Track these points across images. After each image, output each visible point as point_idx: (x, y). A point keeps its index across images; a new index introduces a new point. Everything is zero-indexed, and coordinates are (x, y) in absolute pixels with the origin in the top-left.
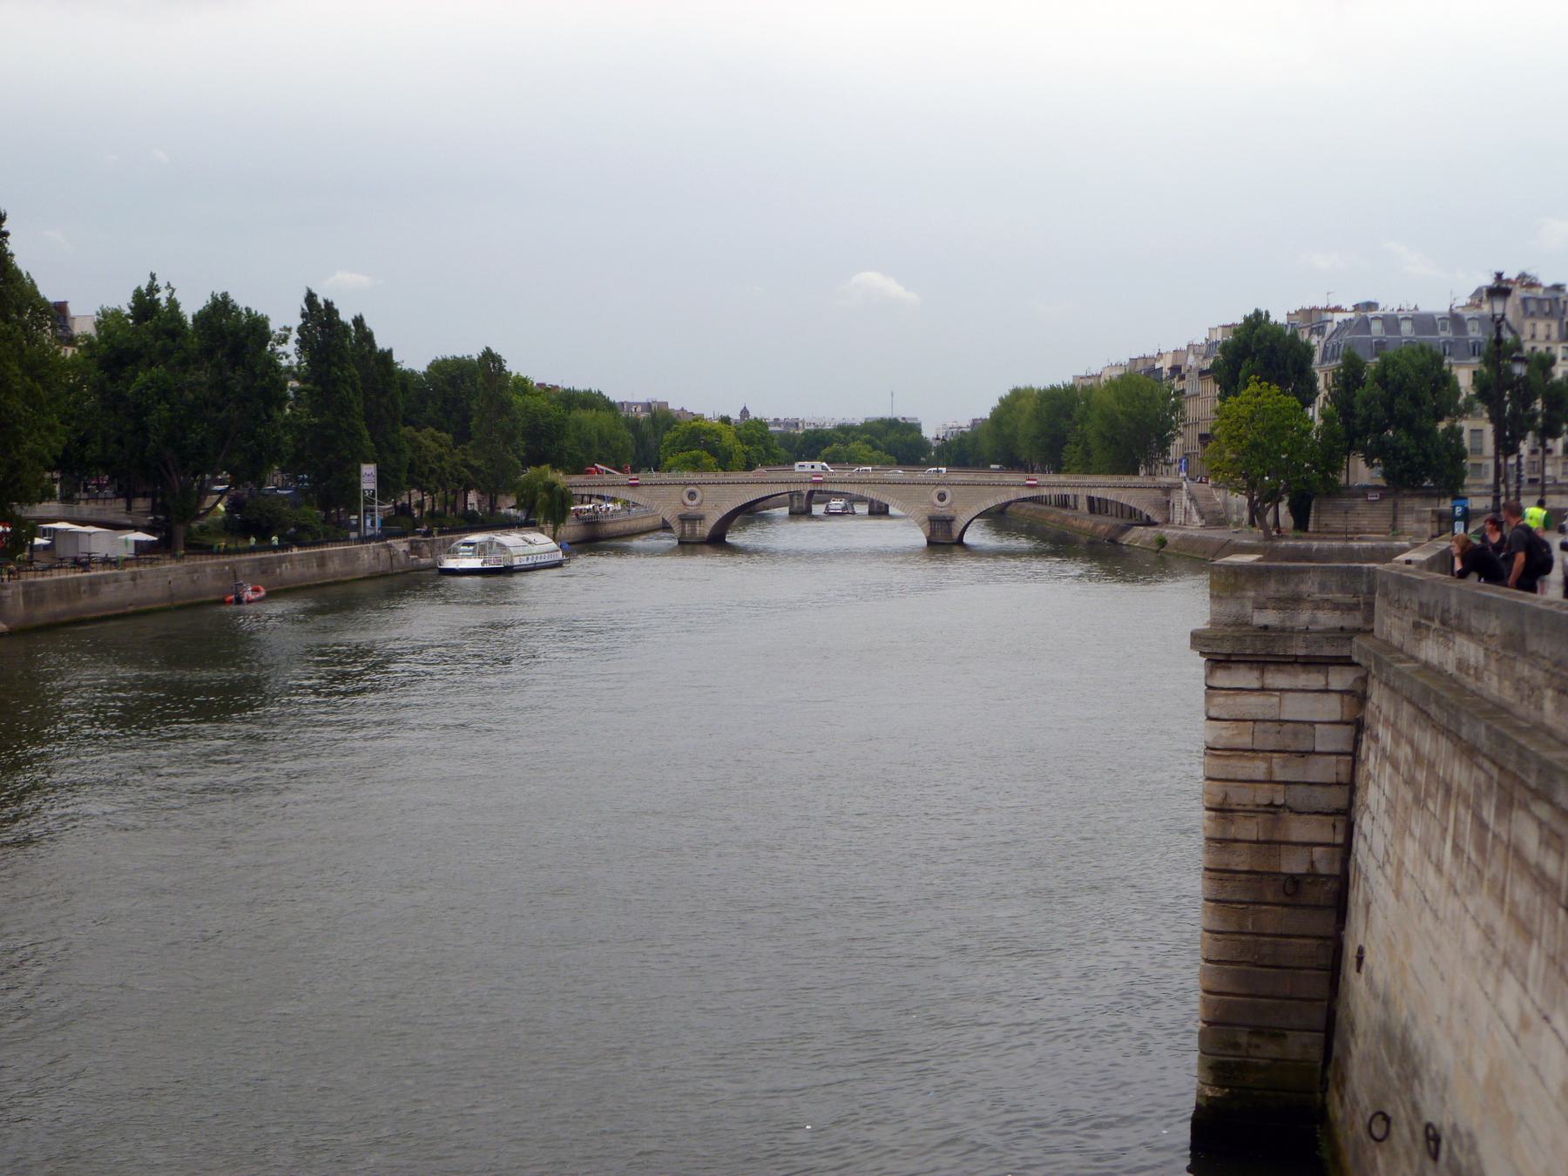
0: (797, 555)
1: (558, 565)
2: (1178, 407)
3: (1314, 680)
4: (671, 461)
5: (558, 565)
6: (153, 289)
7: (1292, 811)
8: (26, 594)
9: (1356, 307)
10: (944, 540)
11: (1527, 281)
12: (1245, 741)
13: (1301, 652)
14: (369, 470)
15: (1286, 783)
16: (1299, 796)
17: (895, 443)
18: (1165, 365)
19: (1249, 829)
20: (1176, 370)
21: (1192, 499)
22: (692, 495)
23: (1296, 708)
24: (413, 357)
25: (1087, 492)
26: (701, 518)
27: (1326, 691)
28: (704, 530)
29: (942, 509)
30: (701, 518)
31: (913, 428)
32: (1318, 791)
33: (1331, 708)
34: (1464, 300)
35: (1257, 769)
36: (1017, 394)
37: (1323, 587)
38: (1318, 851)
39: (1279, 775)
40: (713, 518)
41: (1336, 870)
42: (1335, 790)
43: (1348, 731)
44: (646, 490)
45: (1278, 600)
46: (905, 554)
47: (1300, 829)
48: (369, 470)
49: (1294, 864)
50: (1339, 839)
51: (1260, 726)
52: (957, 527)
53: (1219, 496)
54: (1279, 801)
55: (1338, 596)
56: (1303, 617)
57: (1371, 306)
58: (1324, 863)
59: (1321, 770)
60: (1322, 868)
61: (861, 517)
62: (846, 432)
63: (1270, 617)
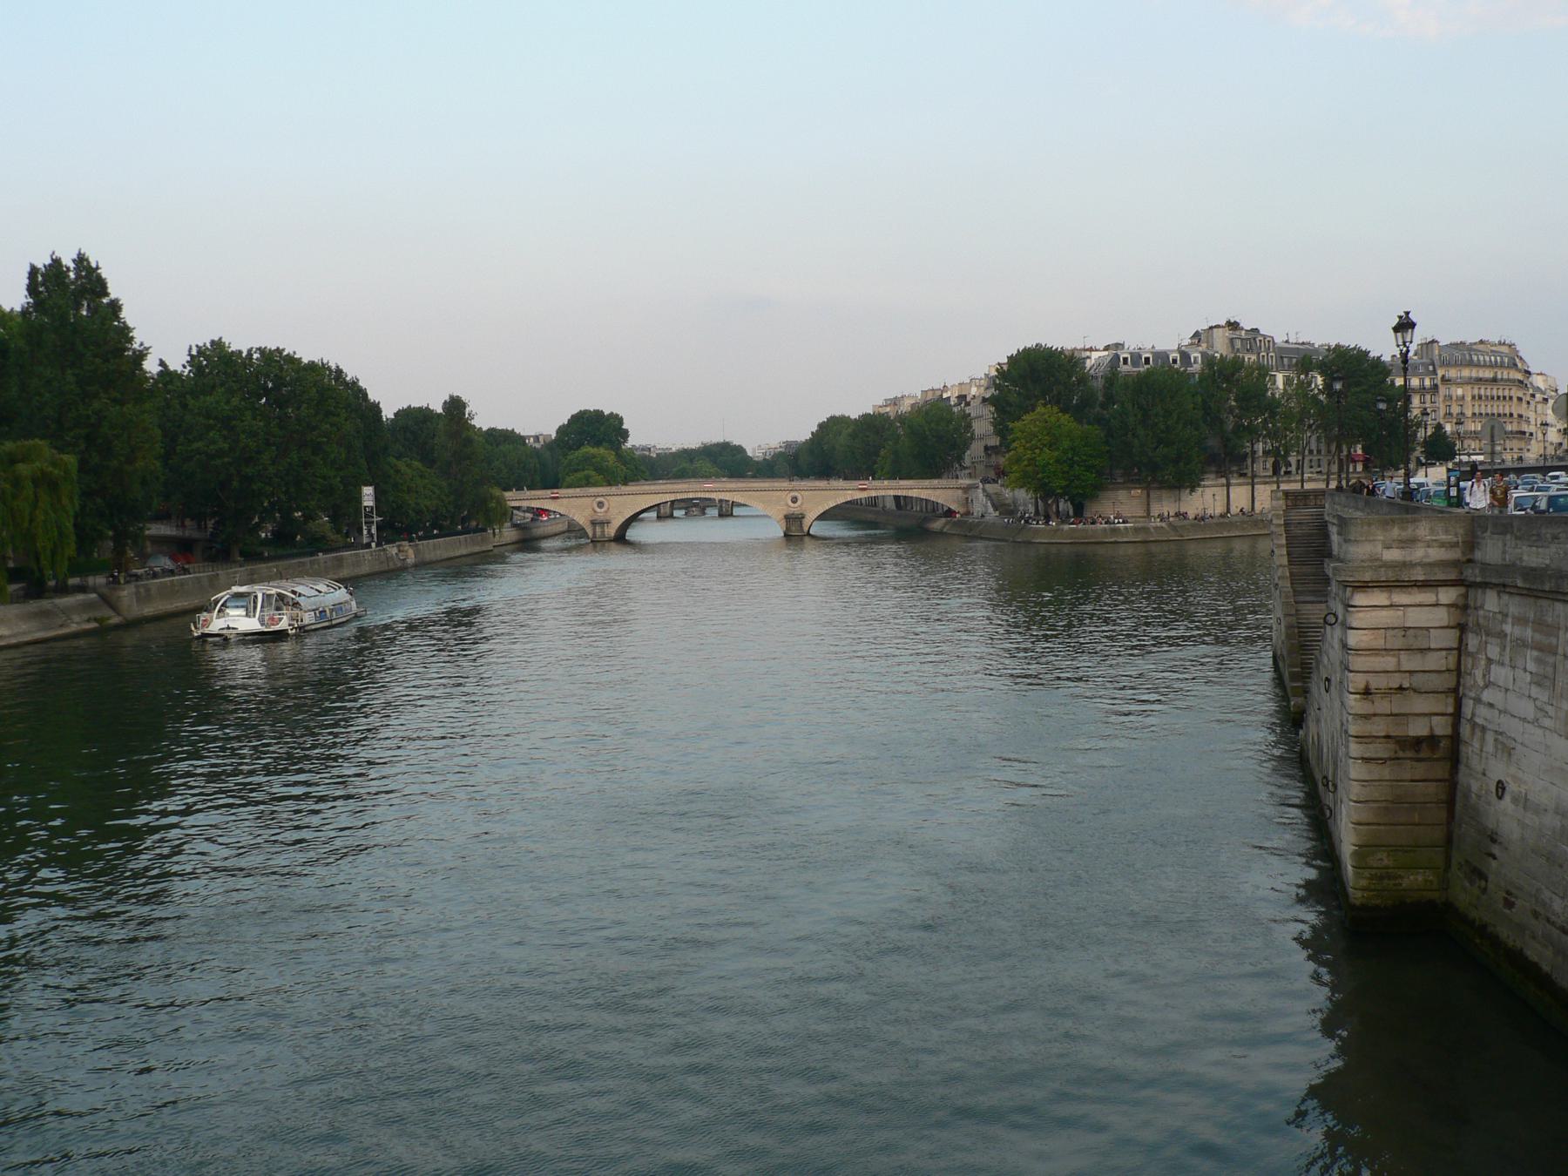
0: (662, 548)
2: (969, 426)
3: (1427, 597)
4: (568, 479)
7: (1415, 691)
9: (1107, 348)
12: (1380, 643)
13: (1421, 578)
14: (368, 491)
15: (1410, 672)
16: (1418, 681)
17: (725, 460)
18: (952, 394)
20: (962, 398)
21: (988, 496)
22: (600, 505)
23: (1416, 618)
24: (391, 397)
25: (892, 493)
27: (1437, 605)
28: (611, 531)
29: (795, 509)
31: (740, 450)
32: (1433, 676)
33: (1441, 617)
34: (1187, 342)
35: (1389, 662)
36: (834, 421)
37: (1432, 531)
38: (1435, 719)
39: (1406, 666)
40: (617, 522)
41: (1449, 731)
42: (1447, 675)
43: (1455, 633)
45: (1401, 541)
46: (766, 546)
47: (1421, 704)
48: (368, 491)
49: (1418, 729)
50: (1450, 710)
51: (1391, 632)
52: (806, 523)
53: (1007, 494)
55: (1443, 537)
56: (1418, 554)
57: (1119, 346)
58: (1441, 727)
59: (1434, 661)
60: (1439, 731)
61: (713, 518)
62: (688, 455)
63: (1393, 555)
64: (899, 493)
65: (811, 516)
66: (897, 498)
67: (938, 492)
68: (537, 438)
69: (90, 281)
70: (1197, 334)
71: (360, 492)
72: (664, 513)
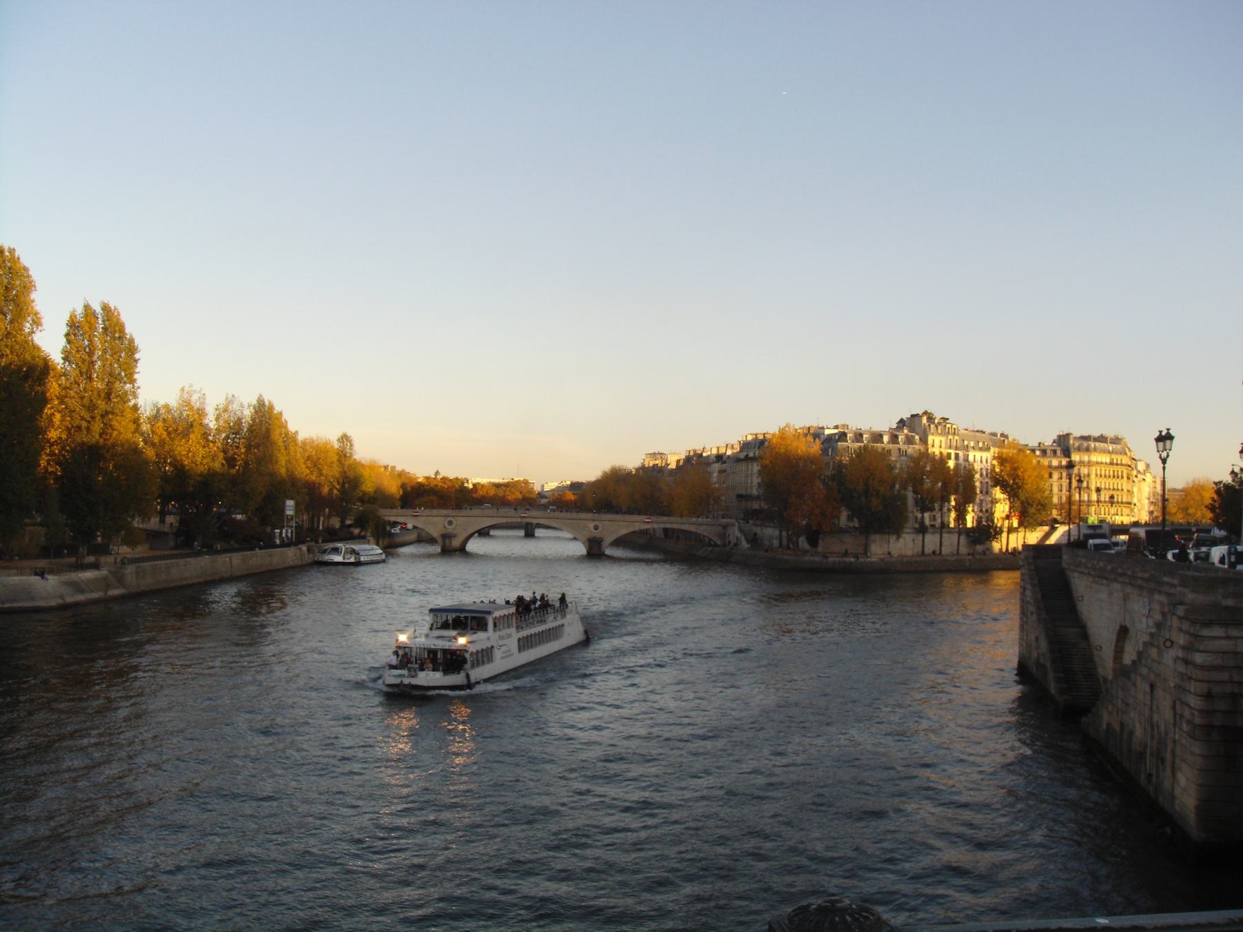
1: (384, 561)
5: (384, 561)
6: (190, 394)
8: (137, 573)
10: (595, 552)
11: (67, 335)
14: (290, 503)
19: (1221, 705)
22: (450, 523)
25: (663, 526)
26: (455, 536)
29: (596, 534)
30: (455, 536)
34: (895, 426)
35: (1225, 676)
39: (1236, 678)
44: (423, 519)
48: (290, 503)
54: (1236, 691)
64: (668, 526)
65: (609, 539)
66: (666, 530)
67: (703, 528)
68: (386, 467)
69: (113, 327)
70: (902, 421)
71: (284, 503)
72: (483, 533)
